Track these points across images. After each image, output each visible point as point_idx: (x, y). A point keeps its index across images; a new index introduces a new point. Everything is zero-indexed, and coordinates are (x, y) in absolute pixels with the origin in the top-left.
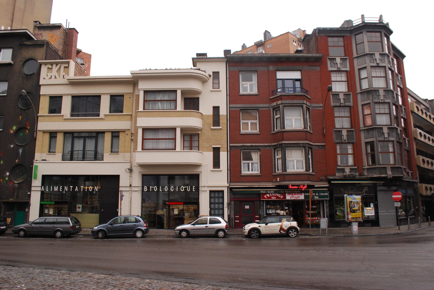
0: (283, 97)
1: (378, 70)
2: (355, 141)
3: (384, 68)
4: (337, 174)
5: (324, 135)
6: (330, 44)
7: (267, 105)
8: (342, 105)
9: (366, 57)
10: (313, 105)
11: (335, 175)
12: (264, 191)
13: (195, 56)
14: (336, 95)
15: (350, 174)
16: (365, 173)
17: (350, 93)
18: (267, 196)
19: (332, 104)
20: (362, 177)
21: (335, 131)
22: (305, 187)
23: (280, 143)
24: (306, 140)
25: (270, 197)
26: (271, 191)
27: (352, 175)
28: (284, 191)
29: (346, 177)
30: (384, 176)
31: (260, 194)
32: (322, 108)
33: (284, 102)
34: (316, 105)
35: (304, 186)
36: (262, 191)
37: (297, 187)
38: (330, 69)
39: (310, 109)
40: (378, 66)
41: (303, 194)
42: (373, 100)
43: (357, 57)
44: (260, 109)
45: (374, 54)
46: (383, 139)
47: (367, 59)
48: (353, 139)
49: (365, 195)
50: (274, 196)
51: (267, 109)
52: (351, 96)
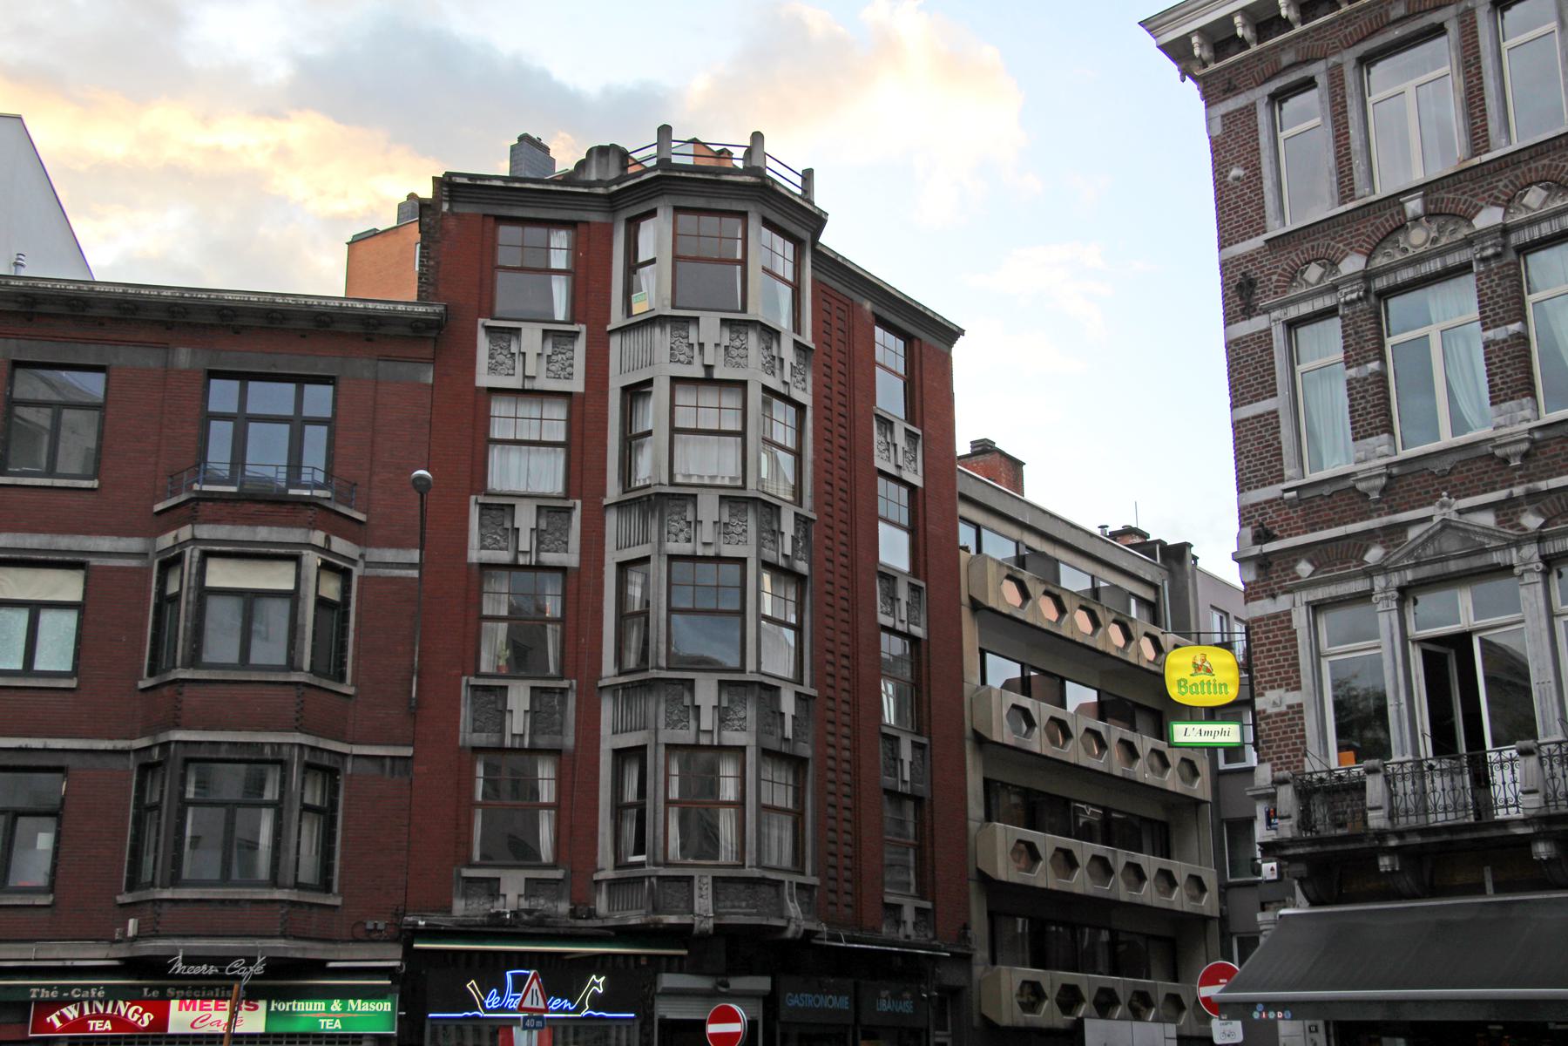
0: (206, 509)
1: (709, 397)
2: (569, 741)
3: (739, 390)
4: (459, 906)
5: (414, 710)
6: (505, 257)
7: (135, 544)
8: (522, 560)
9: (657, 330)
10: (375, 554)
11: (448, 910)
12: (50, 988)
13: (426, 192)
14: (500, 510)
15: (524, 904)
16: (602, 904)
17: (569, 503)
18: (62, 1018)
19: (475, 555)
20: (581, 923)
21: (475, 688)
22: (258, 969)
23: (162, 738)
24: (297, 729)
25: (82, 1023)
26: (88, 987)
27: (529, 912)
28: (163, 989)
29: (503, 923)
30: (673, 919)
31: (26, 1005)
32: (415, 573)
33: (205, 531)
34: (389, 555)
35: (251, 961)
36: (40, 989)
37: (212, 970)
38: (484, 379)
39: (356, 572)
40: (708, 381)
41: (262, 1005)
42: (660, 542)
43: (623, 330)
44: (94, 561)
45: (697, 319)
46: (691, 740)
47: (661, 339)
48: (560, 733)
49: (589, 1017)
50: (104, 1017)
51: (133, 563)
52: (576, 516)
